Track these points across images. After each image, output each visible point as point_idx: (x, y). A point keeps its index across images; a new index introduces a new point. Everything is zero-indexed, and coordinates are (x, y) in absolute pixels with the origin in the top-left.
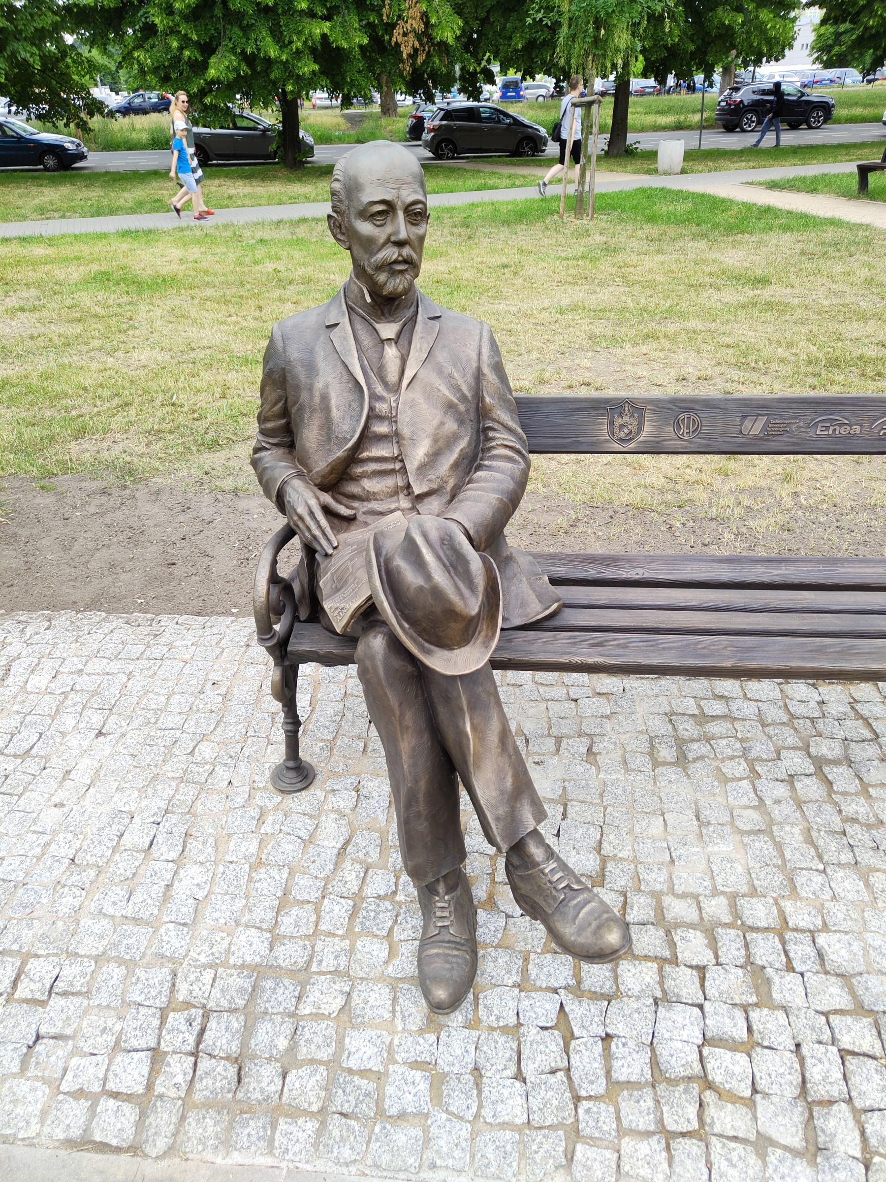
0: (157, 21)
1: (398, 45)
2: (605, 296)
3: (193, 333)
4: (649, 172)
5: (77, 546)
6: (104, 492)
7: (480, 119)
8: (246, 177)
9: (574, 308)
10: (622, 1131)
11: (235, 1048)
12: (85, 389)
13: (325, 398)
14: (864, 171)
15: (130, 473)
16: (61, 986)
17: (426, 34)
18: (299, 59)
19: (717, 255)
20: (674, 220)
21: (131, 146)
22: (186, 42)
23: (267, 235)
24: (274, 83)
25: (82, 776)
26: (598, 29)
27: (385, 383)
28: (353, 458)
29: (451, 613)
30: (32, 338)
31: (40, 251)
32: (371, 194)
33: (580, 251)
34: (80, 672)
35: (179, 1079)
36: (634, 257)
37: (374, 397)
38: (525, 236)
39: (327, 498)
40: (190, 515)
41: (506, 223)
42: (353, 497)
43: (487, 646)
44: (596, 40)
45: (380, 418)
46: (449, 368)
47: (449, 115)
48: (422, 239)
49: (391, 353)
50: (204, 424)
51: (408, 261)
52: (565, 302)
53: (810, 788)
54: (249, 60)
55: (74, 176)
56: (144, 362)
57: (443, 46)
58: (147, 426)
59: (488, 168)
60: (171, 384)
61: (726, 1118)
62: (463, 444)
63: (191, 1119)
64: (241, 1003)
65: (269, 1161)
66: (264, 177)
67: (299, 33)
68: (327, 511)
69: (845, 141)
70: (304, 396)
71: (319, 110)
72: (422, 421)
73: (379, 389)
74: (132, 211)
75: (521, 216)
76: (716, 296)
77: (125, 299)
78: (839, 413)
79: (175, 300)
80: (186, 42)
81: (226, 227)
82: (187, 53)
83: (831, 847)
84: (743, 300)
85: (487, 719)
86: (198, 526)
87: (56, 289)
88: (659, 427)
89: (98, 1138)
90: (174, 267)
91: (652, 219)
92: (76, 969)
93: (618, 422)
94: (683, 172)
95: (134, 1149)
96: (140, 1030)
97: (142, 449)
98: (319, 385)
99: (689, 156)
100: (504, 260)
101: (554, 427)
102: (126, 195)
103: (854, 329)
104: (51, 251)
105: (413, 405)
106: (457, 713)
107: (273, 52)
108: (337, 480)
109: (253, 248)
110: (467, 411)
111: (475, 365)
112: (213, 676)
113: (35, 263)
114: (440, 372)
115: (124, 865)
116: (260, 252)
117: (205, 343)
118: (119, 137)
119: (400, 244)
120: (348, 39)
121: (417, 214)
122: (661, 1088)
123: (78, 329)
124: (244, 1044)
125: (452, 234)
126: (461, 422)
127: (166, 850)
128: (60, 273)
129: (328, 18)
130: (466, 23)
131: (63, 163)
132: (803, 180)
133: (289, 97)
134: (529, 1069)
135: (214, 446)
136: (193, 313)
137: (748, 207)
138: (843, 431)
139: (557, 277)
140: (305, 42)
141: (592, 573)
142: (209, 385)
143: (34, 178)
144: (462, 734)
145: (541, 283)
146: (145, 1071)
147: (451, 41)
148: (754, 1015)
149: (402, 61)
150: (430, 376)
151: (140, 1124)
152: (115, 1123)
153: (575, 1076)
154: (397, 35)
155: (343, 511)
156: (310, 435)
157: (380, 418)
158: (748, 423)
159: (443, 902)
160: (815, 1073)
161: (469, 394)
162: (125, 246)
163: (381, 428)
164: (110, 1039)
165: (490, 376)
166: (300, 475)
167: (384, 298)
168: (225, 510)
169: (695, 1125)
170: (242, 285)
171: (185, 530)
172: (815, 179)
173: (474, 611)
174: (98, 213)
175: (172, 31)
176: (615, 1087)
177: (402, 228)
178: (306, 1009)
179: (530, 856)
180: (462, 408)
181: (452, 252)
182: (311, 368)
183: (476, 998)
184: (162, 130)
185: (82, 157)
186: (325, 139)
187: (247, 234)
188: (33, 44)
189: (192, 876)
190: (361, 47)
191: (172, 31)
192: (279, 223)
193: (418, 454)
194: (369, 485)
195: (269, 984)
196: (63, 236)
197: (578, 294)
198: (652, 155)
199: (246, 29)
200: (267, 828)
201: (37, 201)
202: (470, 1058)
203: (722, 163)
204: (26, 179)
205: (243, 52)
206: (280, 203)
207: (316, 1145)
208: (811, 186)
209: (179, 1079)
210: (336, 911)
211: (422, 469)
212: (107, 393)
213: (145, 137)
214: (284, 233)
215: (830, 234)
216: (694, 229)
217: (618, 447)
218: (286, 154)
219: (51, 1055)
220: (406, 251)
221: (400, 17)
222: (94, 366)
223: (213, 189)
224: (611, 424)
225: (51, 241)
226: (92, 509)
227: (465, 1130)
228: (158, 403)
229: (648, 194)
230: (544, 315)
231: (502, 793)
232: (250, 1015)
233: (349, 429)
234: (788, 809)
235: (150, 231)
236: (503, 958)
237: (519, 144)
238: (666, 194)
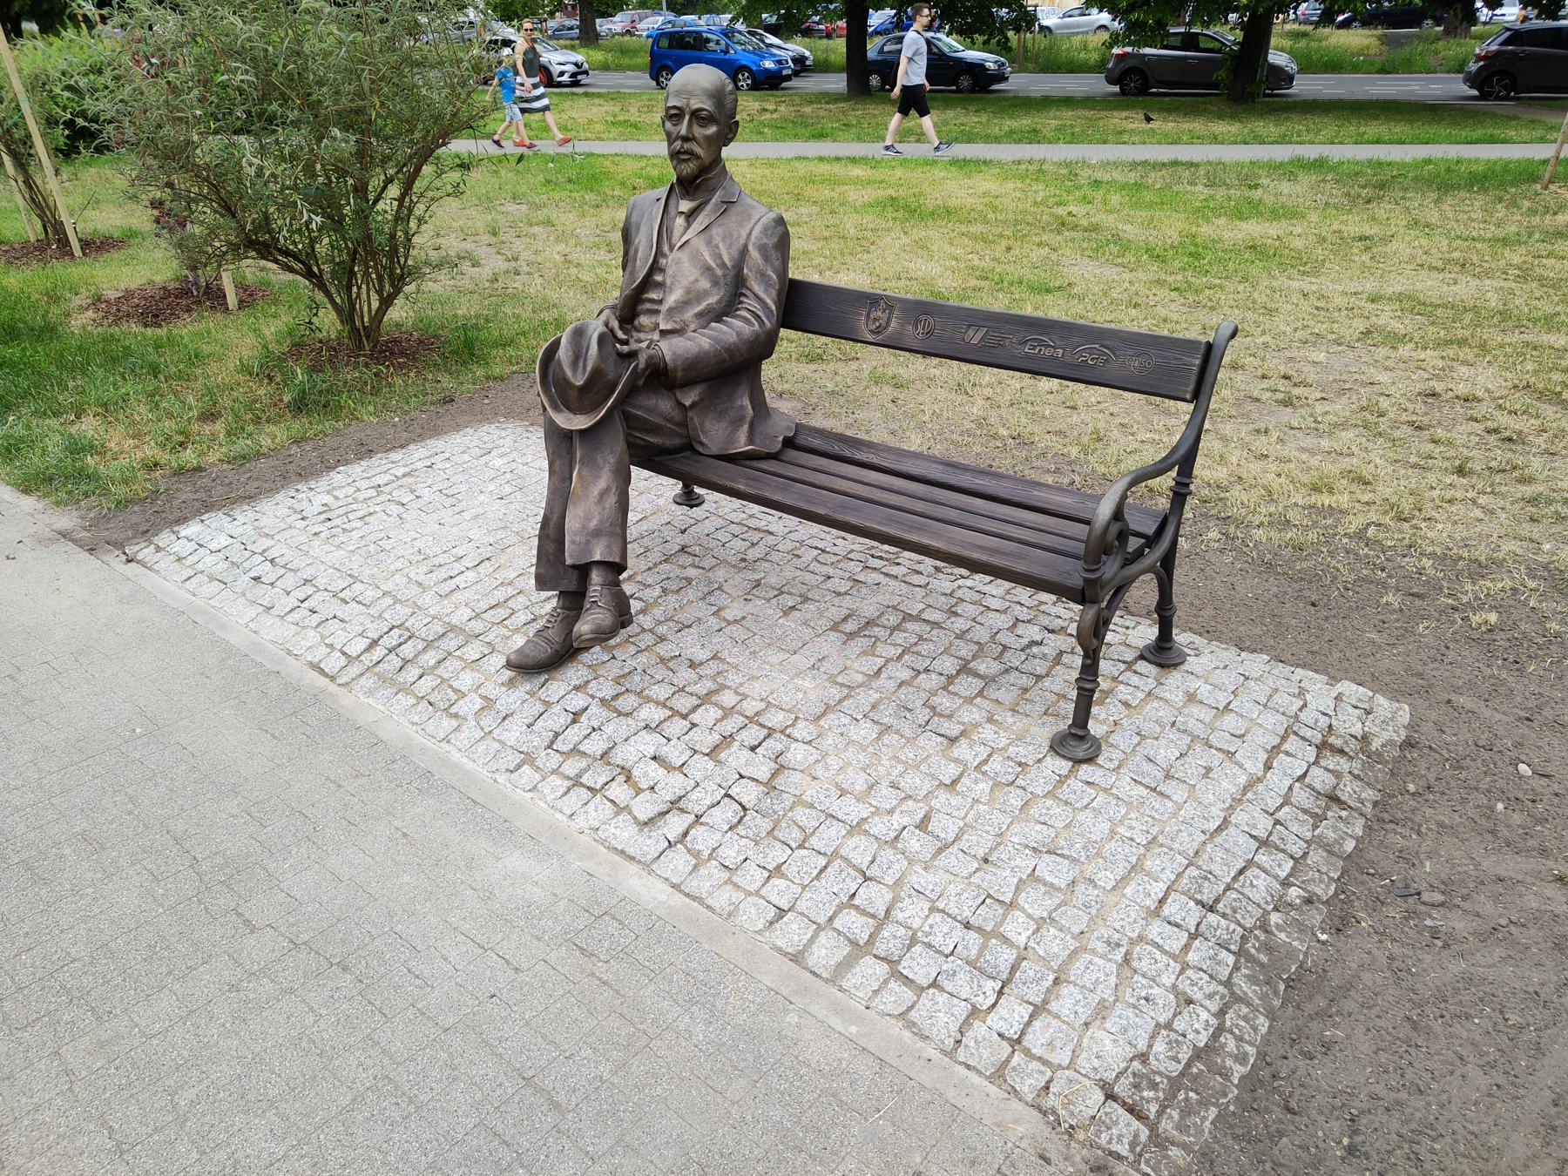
61: (619, 791)
62: (712, 300)
78: (1047, 334)
88: (902, 325)
95: (333, 679)
101: (802, 307)
105: (678, 262)
110: (724, 276)
111: (742, 241)
114: (709, 243)
126: (715, 283)
138: (1047, 352)
141: (836, 449)
158: (971, 332)
161: (729, 264)
163: (658, 278)
180: (719, 272)
185: (1002, 78)
189: (471, 575)
217: (870, 338)
224: (868, 316)
227: (478, 734)
231: (584, 527)
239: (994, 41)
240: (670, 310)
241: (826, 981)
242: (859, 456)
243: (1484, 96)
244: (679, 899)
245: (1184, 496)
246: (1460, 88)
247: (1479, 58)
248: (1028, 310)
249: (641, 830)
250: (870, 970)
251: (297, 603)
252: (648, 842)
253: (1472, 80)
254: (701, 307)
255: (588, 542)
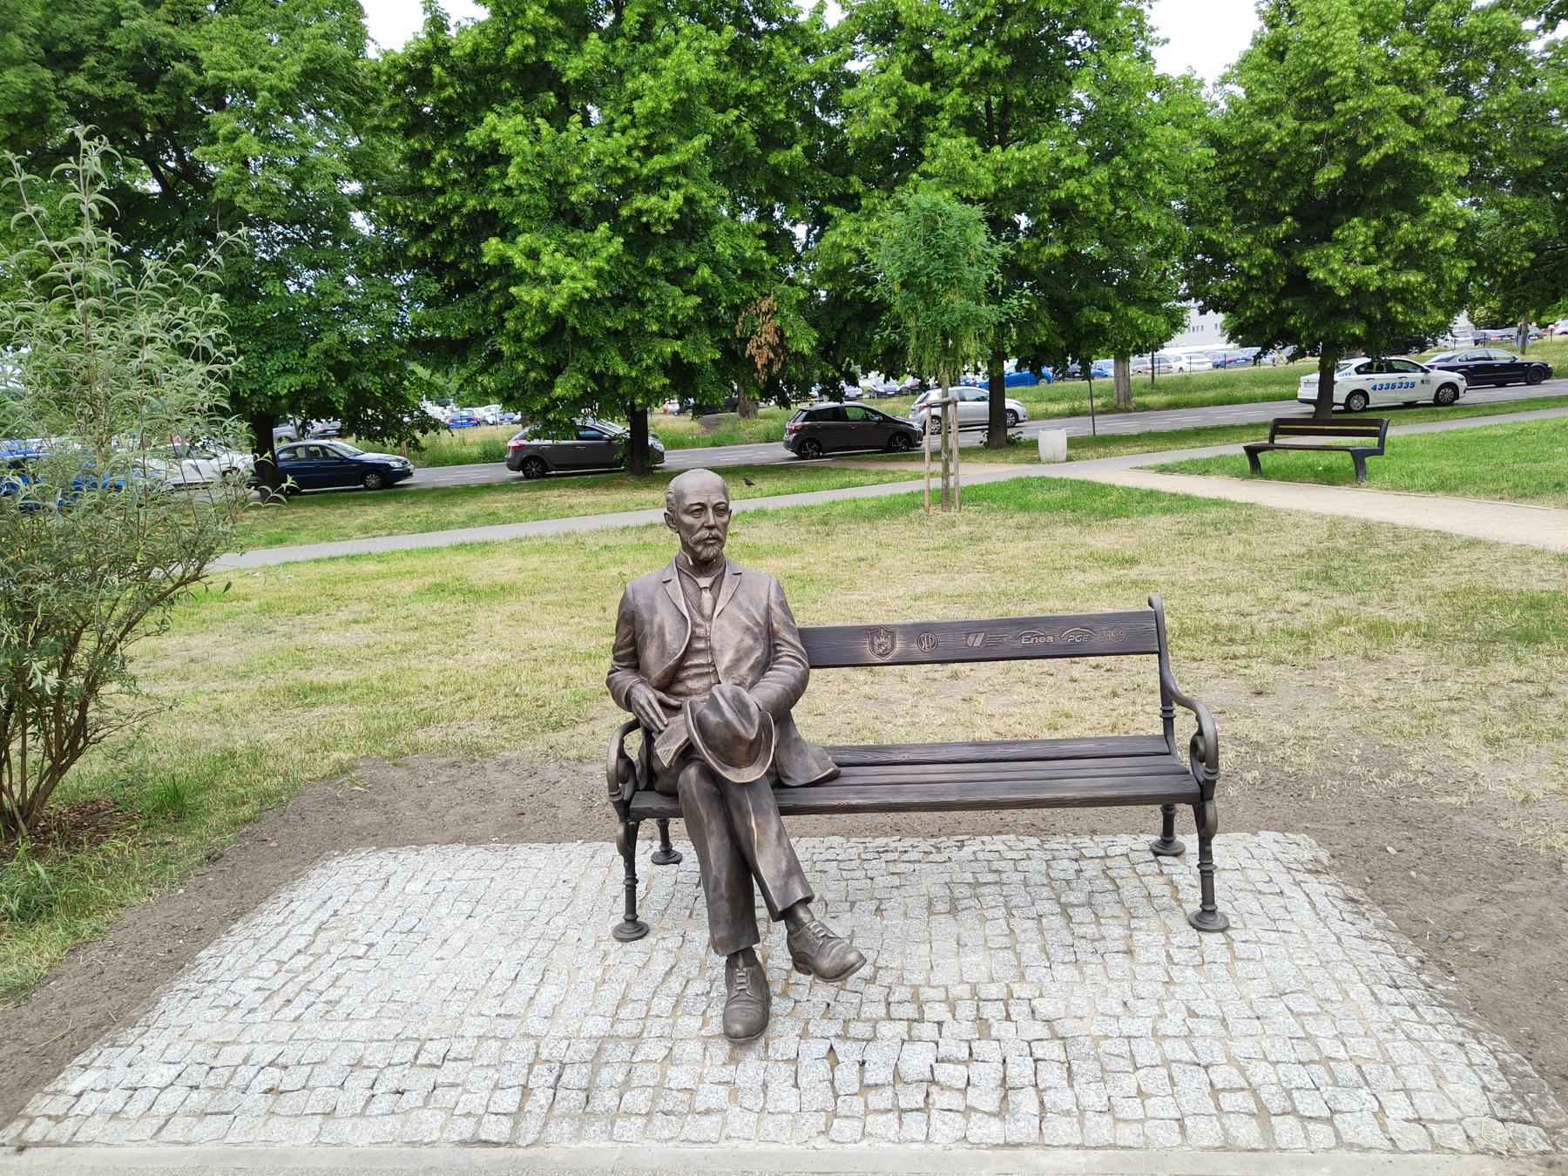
0: (504, 348)
1: (752, 357)
2: (962, 582)
3: (534, 634)
4: (1030, 462)
5: (432, 806)
6: (453, 765)
7: (847, 419)
8: (589, 487)
9: (930, 595)
10: (867, 1112)
11: (584, 1084)
12: (426, 687)
13: (661, 628)
14: (1252, 452)
15: (478, 749)
16: (452, 1055)
17: (781, 345)
18: (649, 375)
19: (1089, 540)
20: (1049, 507)
21: (460, 461)
22: (532, 365)
23: (611, 542)
24: (623, 397)
25: (457, 940)
26: (946, 340)
27: (702, 616)
28: (680, 666)
29: (738, 738)
30: (368, 646)
31: (370, 567)
32: (691, 500)
33: (941, 541)
34: (450, 879)
35: (543, 1102)
36: (999, 545)
37: (695, 625)
38: (885, 531)
39: (661, 695)
40: (536, 779)
41: (867, 518)
42: (680, 694)
43: (764, 765)
44: (945, 349)
45: (699, 638)
46: (747, 605)
47: (811, 416)
48: (725, 525)
49: (707, 596)
50: (548, 709)
51: (716, 538)
52: (920, 589)
53: (1056, 922)
54: (597, 378)
55: (396, 494)
56: (484, 661)
57: (799, 357)
58: (493, 712)
59: (855, 466)
60: (514, 678)
62: (758, 654)
63: (552, 1124)
64: (589, 1058)
65: (609, 1144)
66: (608, 485)
67: (650, 352)
68: (662, 704)
69: (1255, 421)
70: (647, 627)
71: (667, 419)
72: (728, 637)
73: (699, 620)
74: (464, 525)
75: (885, 510)
76: (1080, 576)
77: (461, 607)
79: (515, 606)
80: (532, 365)
81: (567, 535)
82: (533, 375)
83: (1060, 954)
84: (1107, 579)
85: (768, 822)
86: (545, 786)
87: (390, 601)
88: (907, 645)
89: (483, 1137)
90: (513, 576)
91: (1024, 508)
92: (463, 1044)
93: (877, 642)
94: (1069, 459)
95: (509, 1144)
96: (513, 1075)
97: (487, 732)
98: (657, 619)
99: (1073, 443)
100: (861, 554)
101: (829, 649)
102: (457, 510)
103: (1218, 601)
104: (379, 567)
105: (721, 628)
106: (745, 815)
107: (622, 370)
108: (669, 682)
109: (596, 554)
112: (564, 877)
113: (365, 579)
114: (741, 607)
115: (496, 987)
116: (604, 558)
117: (547, 643)
118: (447, 452)
119: (711, 528)
120: (700, 355)
121: (722, 510)
122: (899, 1086)
123: (415, 636)
124: (592, 1081)
125: (809, 532)
126: (756, 640)
127: (528, 981)
128: (392, 586)
129: (679, 337)
130: (822, 334)
131: (386, 481)
132: (1193, 462)
133: (638, 409)
134: (802, 1082)
135: (558, 726)
136: (534, 616)
137: (1129, 492)
139: (915, 567)
140: (655, 360)
141: (869, 757)
142: (552, 678)
143: (356, 498)
144: (749, 829)
145: (824, 550)
146: (518, 1098)
147: (806, 351)
148: (974, 1045)
149: (757, 370)
150: (733, 610)
151: (514, 1128)
152: (495, 1129)
153: (837, 1084)
154: (751, 349)
155: (673, 702)
156: (651, 654)
157: (699, 638)
158: (971, 638)
159: (742, 972)
160: (1013, 1071)
162: (459, 559)
163: (700, 645)
164: (491, 1084)
165: (777, 610)
166: (642, 682)
167: (703, 562)
168: (569, 774)
169: (922, 1105)
170: (585, 588)
171: (532, 789)
172: (1208, 461)
173: (753, 737)
174: (428, 528)
175: (520, 356)
176: (865, 1087)
177: (711, 518)
178: (637, 1059)
179: (800, 920)
181: (808, 549)
182: (652, 609)
183: (767, 1045)
184: (495, 443)
185: (408, 474)
186: (677, 443)
187: (590, 541)
188: (375, 374)
190: (713, 361)
191: (520, 356)
192: (624, 529)
193: (725, 660)
194: (691, 684)
195: (611, 1046)
196: (393, 552)
197: (935, 582)
198: (1033, 445)
199: (595, 351)
200: (610, 961)
201: (360, 520)
202: (760, 1079)
203: (1113, 449)
204: (347, 500)
205: (591, 372)
206: (626, 510)
207: (644, 1132)
208: (1202, 469)
209: (543, 1102)
210: (663, 1004)
211: (728, 670)
212: (448, 689)
213: (476, 451)
214: (630, 539)
215: (1213, 514)
216: (1069, 516)
217: (879, 660)
218: (636, 461)
219: (447, 1097)
220: (714, 532)
221: (753, 332)
222: (434, 667)
223: (552, 499)
224: (872, 643)
225: (380, 558)
226: (444, 779)
227: (753, 1117)
228: (501, 694)
229: (1024, 484)
230: (899, 602)
232: (596, 1062)
233: (676, 647)
234: (1033, 935)
235: (486, 544)
236: (789, 1023)
237: (894, 440)
238: (1044, 482)
239: (404, 444)
240: (727, 669)
241: (1266, 1150)
242: (894, 758)
243: (802, 457)
244: (1096, 1156)
245: (1171, 719)
246: (780, 452)
247: (791, 432)
248: (1014, 615)
249: (1004, 1119)
250: (1285, 1128)
251: (368, 1093)
252: (1021, 1124)
253: (788, 445)
254: (752, 661)
255: (786, 884)
